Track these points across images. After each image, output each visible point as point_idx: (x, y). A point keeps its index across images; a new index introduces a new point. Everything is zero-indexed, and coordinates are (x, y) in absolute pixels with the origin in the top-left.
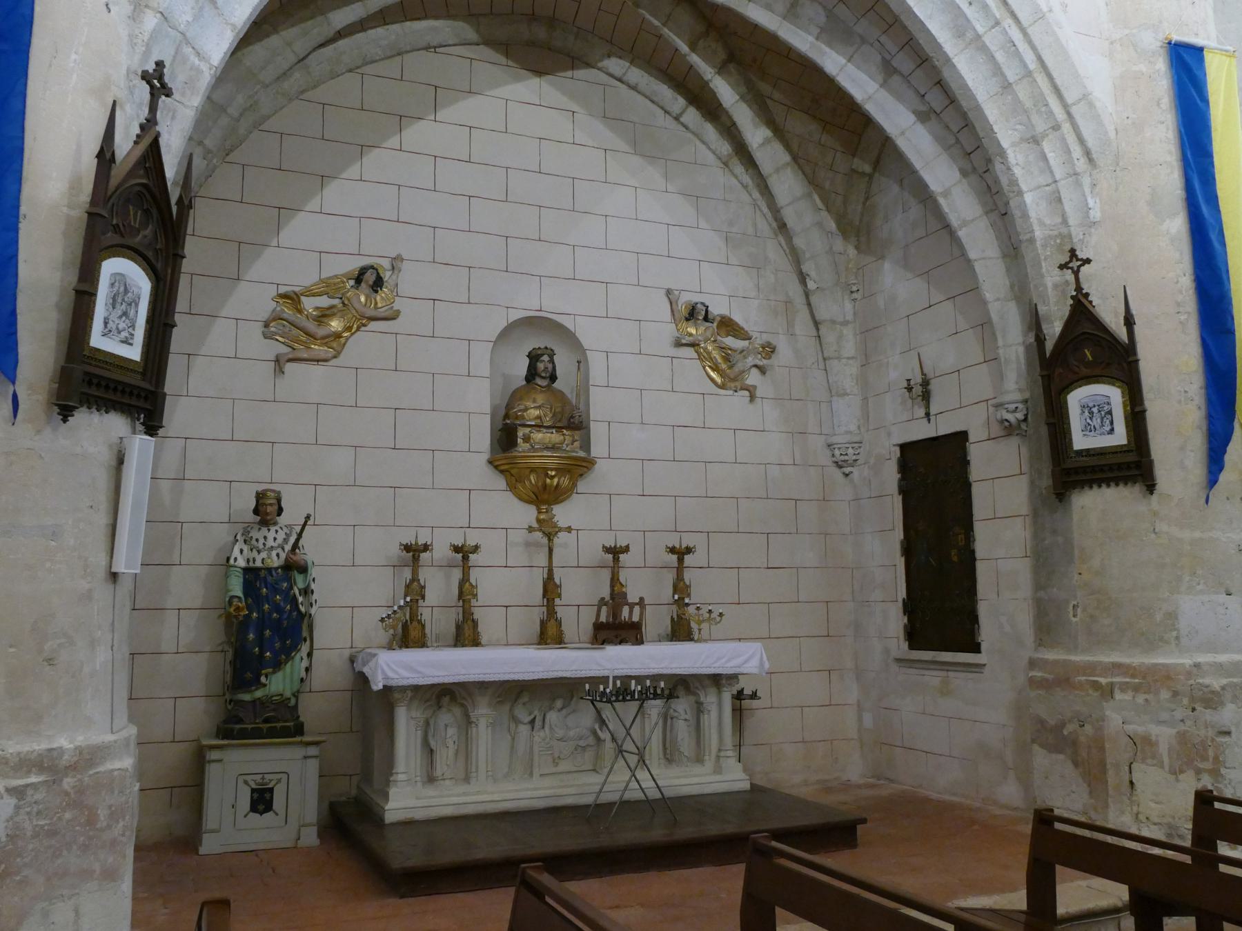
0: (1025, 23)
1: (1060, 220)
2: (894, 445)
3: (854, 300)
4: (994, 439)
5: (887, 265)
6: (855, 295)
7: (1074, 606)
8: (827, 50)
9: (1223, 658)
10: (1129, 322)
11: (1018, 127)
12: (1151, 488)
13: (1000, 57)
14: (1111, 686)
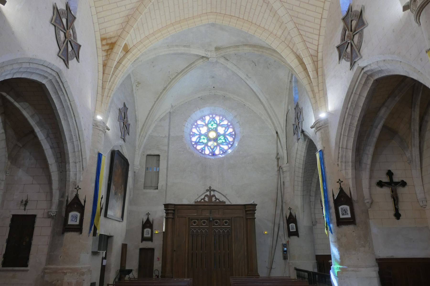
0: (81, 142)
1: (75, 179)
2: (11, 214)
3: (6, 175)
4: (44, 218)
5: (20, 170)
6: (7, 174)
7: (60, 256)
8: (37, 127)
9: (85, 266)
10: (85, 202)
11: (74, 159)
12: (81, 233)
13: (75, 146)
14: (66, 273)
